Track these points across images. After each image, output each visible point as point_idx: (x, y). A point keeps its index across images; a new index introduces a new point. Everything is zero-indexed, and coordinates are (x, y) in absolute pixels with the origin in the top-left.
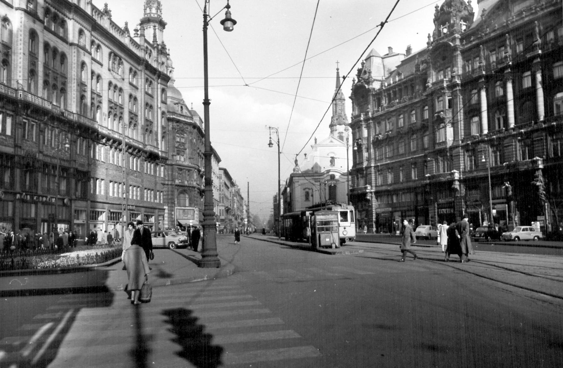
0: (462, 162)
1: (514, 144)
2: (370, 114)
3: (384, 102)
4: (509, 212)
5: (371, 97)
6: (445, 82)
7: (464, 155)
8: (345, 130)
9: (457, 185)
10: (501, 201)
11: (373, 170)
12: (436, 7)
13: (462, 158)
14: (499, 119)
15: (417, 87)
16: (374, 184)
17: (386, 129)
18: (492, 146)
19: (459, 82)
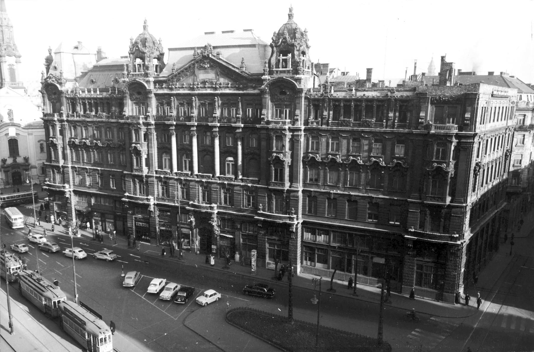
0: (156, 190)
1: (197, 187)
2: (64, 116)
3: (80, 109)
4: (192, 236)
5: (64, 99)
6: (141, 119)
7: (158, 184)
8: (16, 62)
9: (152, 208)
10: (186, 226)
11: (70, 170)
12: (131, 40)
13: (156, 186)
14: (185, 161)
15: (114, 108)
16: (71, 183)
17: (82, 136)
18: (181, 183)
19: (153, 122)
